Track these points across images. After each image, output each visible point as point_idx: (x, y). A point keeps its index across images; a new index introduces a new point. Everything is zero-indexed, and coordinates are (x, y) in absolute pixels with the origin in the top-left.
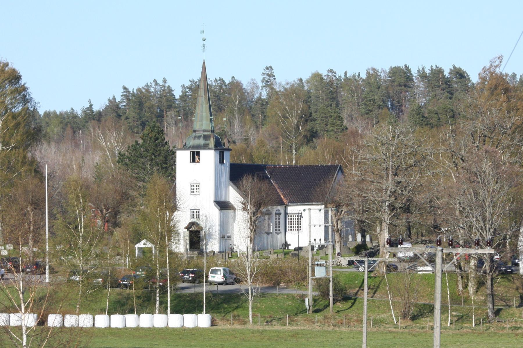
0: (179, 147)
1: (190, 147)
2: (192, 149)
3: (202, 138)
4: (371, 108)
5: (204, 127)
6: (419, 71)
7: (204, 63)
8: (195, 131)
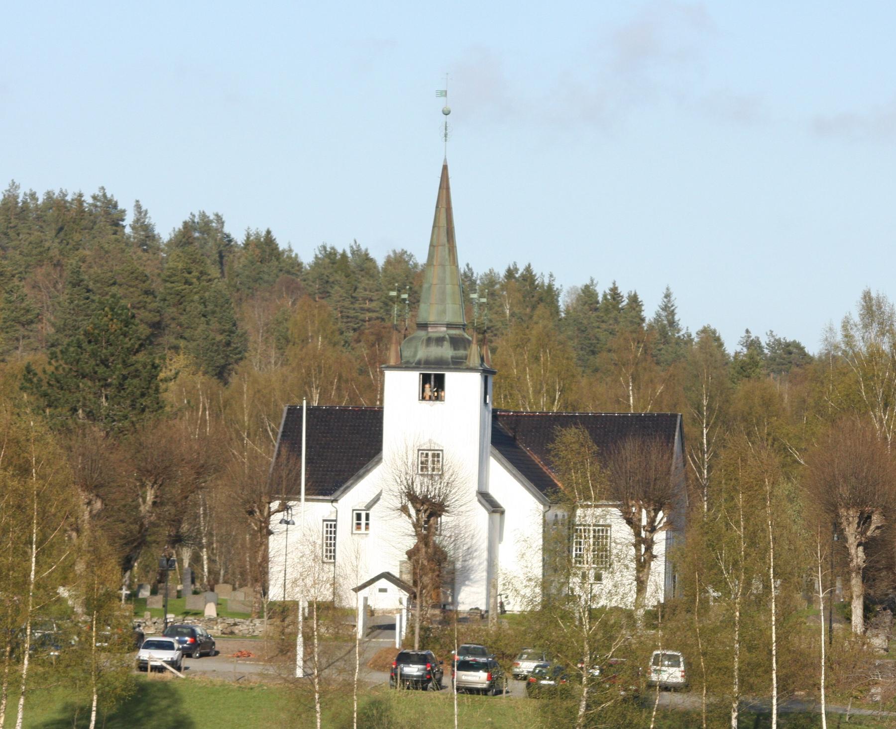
2: (425, 368)
3: (446, 344)
5: (449, 318)
7: (445, 168)
8: (424, 326)
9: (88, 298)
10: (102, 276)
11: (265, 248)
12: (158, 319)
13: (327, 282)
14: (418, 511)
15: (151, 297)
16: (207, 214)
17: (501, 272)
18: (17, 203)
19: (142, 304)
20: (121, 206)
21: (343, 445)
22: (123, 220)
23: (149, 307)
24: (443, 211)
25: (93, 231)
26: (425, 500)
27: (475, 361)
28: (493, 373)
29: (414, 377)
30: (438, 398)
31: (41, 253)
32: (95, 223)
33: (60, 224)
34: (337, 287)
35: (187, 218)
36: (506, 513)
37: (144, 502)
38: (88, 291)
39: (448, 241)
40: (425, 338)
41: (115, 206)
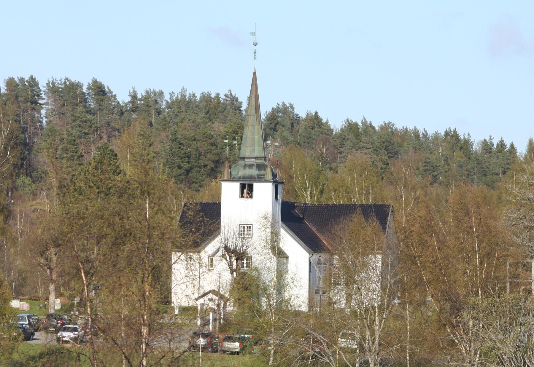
0: (225, 178)
1: (240, 178)
3: (254, 168)
4: (86, 131)
5: (256, 154)
6: (48, 84)
7: (255, 74)
8: (243, 158)
9: (180, 148)
10: (188, 136)
11: (315, 121)
12: (217, 158)
13: (344, 139)
14: (230, 257)
15: (214, 147)
16: (286, 104)
17: (442, 133)
18: (186, 99)
19: (209, 151)
20: (239, 100)
21: (204, 221)
22: (241, 107)
23: (213, 152)
24: (253, 96)
25: (224, 113)
26: (234, 252)
27: (269, 176)
28: (282, 183)
29: (236, 186)
30: (251, 197)
31: (165, 125)
32: (225, 110)
33: (207, 110)
34: (348, 142)
35: (275, 106)
36: (289, 258)
37: (93, 253)
38: (180, 144)
39: (256, 113)
40: (243, 164)
41: (237, 100)
